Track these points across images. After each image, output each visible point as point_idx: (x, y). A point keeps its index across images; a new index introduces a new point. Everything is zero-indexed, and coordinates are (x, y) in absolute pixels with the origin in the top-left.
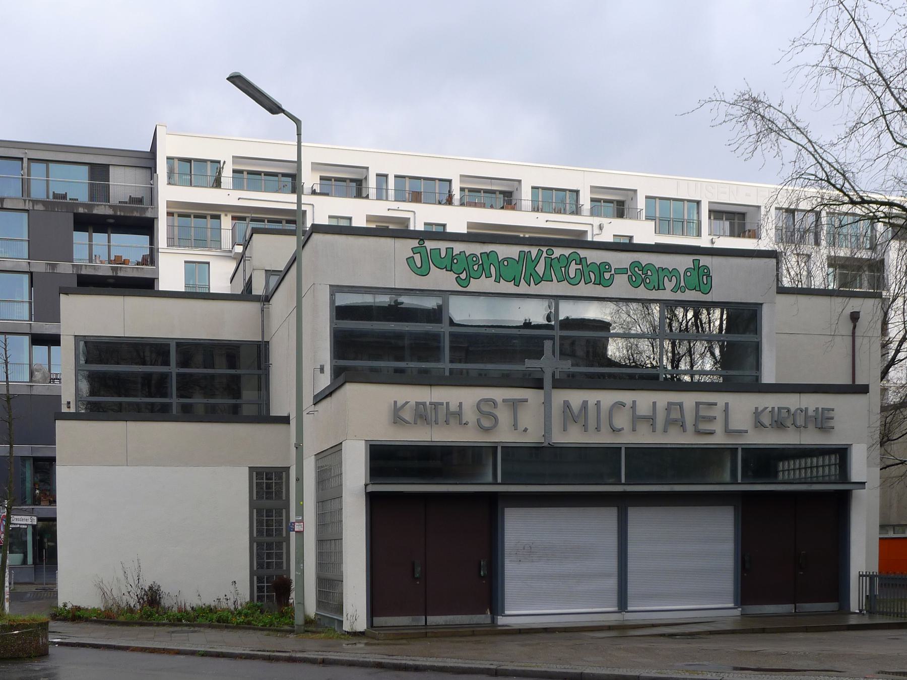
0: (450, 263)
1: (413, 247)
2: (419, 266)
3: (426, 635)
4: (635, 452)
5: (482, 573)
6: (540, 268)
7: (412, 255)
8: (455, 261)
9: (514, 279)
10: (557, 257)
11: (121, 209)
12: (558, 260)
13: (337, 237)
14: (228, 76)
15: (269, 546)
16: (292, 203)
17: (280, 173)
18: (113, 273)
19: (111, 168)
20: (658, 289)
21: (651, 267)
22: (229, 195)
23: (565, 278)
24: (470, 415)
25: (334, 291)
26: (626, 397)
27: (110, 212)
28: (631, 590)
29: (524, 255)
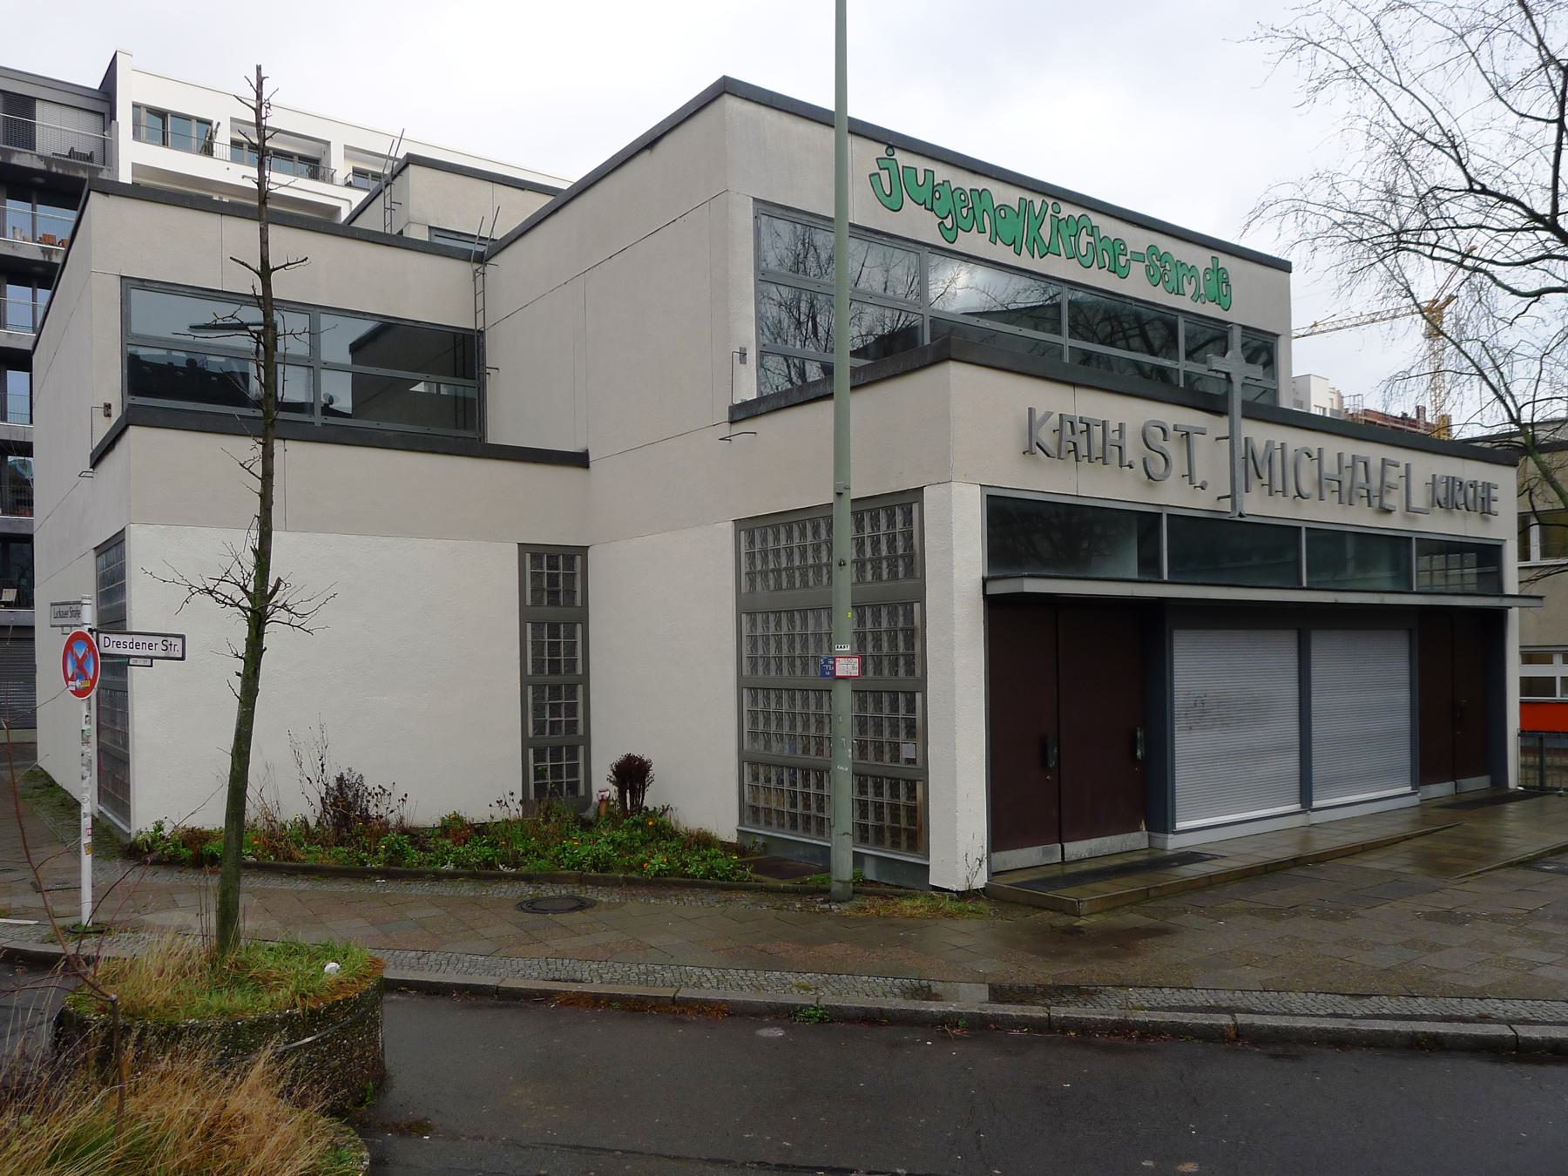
0: (931, 197)
1: (879, 156)
2: (888, 193)
3: (1148, 894)
5: (1139, 753)
6: (1046, 231)
8: (937, 195)
9: (1014, 242)
10: (1064, 219)
11: (60, 163)
12: (1067, 222)
13: (763, 110)
15: (555, 691)
16: (321, 194)
17: (296, 154)
18: (44, 257)
19: (38, 104)
21: (1169, 259)
22: (228, 169)
25: (760, 211)
27: (41, 166)
28: (1318, 771)
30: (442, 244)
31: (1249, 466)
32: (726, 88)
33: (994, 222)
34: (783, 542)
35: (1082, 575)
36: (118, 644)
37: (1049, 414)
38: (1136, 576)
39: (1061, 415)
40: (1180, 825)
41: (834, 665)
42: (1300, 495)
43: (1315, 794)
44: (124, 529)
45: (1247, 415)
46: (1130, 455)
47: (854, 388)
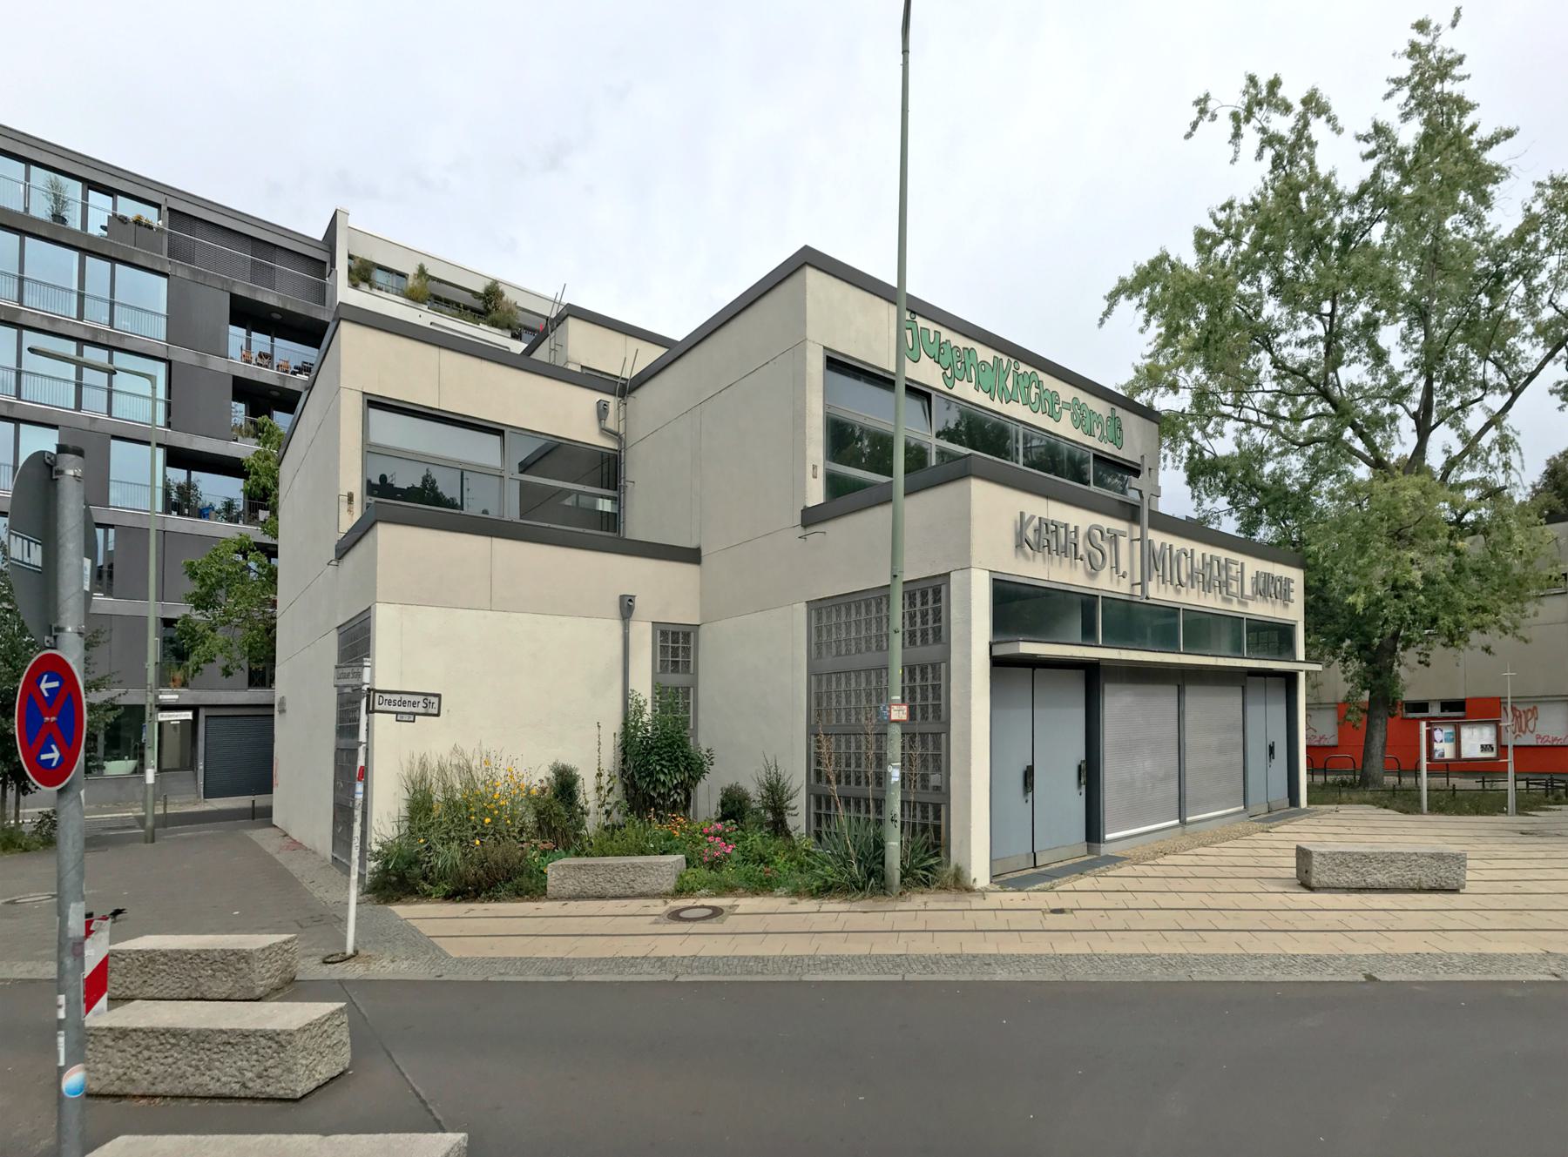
6: (1010, 383)
28: (1190, 793)
30: (590, 379)
31: (1152, 561)
32: (808, 259)
33: (977, 375)
34: (843, 618)
35: (1055, 640)
36: (390, 702)
37: (1033, 517)
38: (1080, 641)
39: (1040, 518)
40: (1108, 837)
41: (890, 711)
42: (1180, 584)
43: (1188, 811)
44: (370, 608)
45: (1153, 526)
46: (1081, 551)
47: (907, 494)
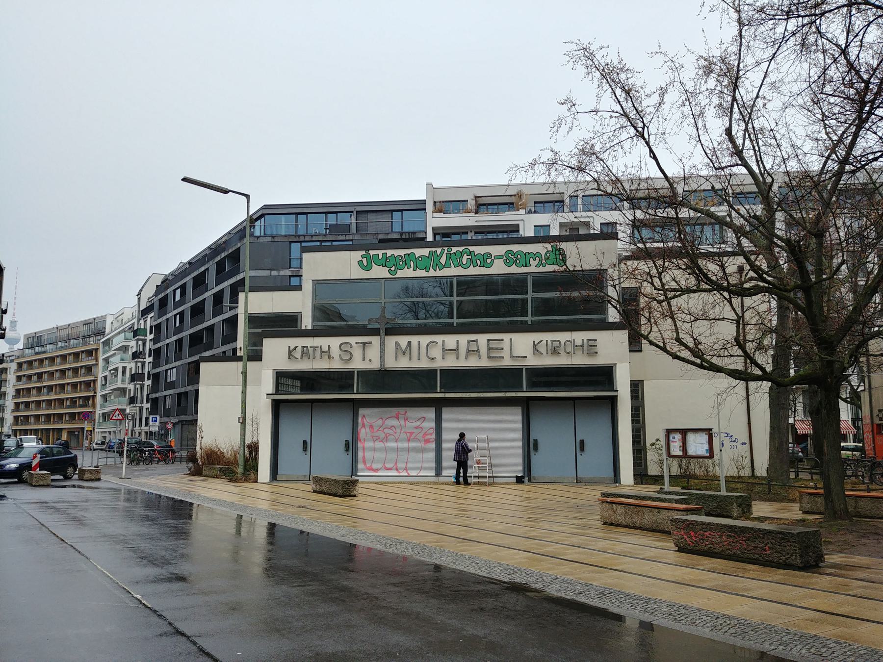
4: (445, 372)
7: (361, 259)
14: (183, 178)
20: (526, 266)
23: (460, 264)
24: (335, 352)
26: (439, 338)
29: (432, 254)
